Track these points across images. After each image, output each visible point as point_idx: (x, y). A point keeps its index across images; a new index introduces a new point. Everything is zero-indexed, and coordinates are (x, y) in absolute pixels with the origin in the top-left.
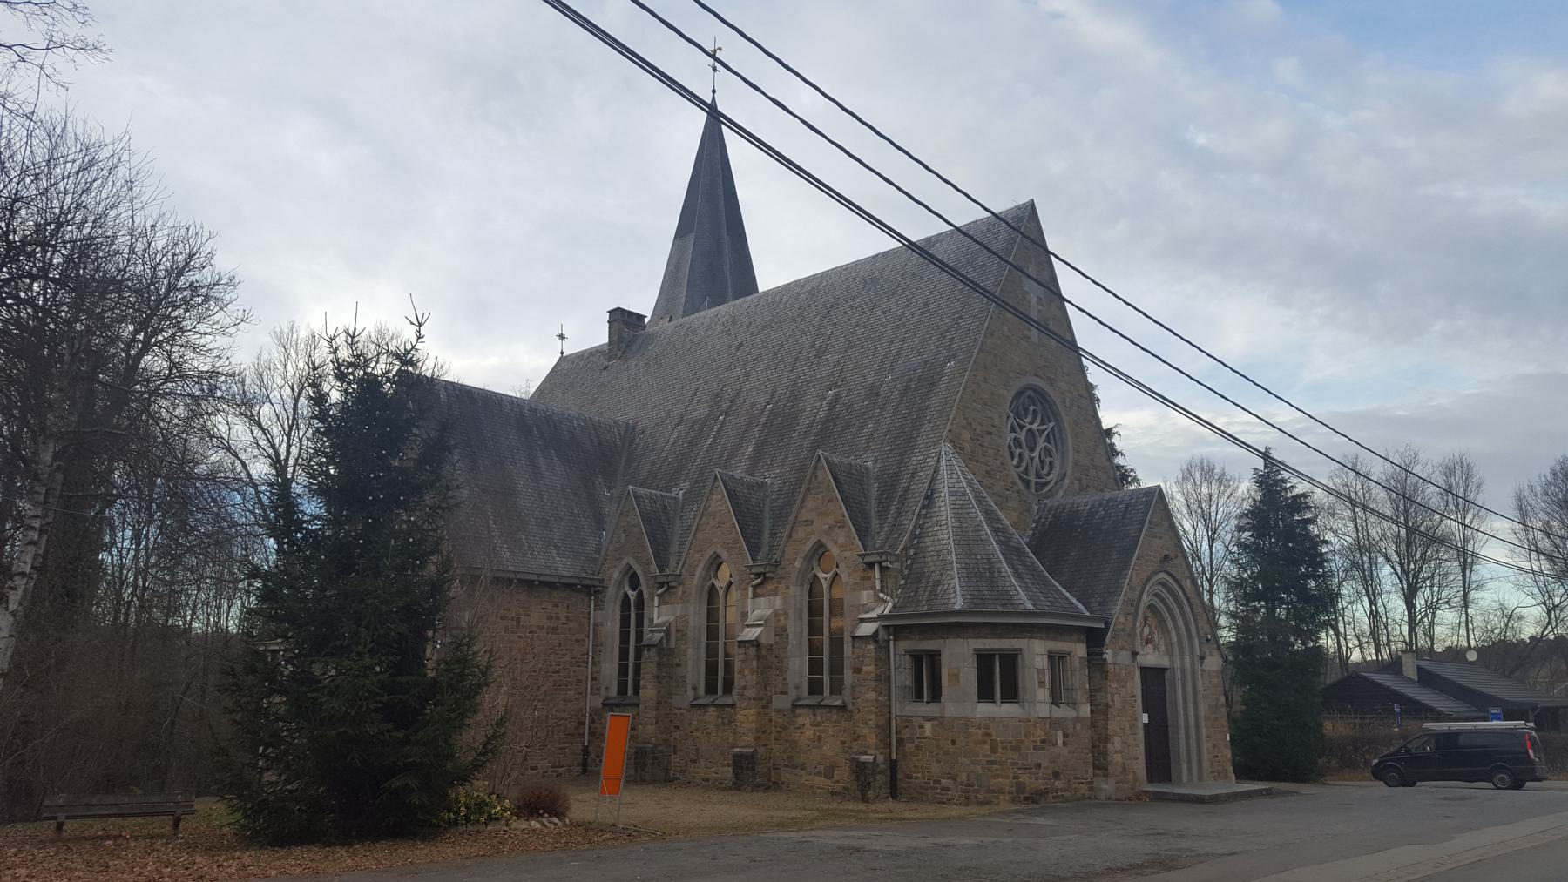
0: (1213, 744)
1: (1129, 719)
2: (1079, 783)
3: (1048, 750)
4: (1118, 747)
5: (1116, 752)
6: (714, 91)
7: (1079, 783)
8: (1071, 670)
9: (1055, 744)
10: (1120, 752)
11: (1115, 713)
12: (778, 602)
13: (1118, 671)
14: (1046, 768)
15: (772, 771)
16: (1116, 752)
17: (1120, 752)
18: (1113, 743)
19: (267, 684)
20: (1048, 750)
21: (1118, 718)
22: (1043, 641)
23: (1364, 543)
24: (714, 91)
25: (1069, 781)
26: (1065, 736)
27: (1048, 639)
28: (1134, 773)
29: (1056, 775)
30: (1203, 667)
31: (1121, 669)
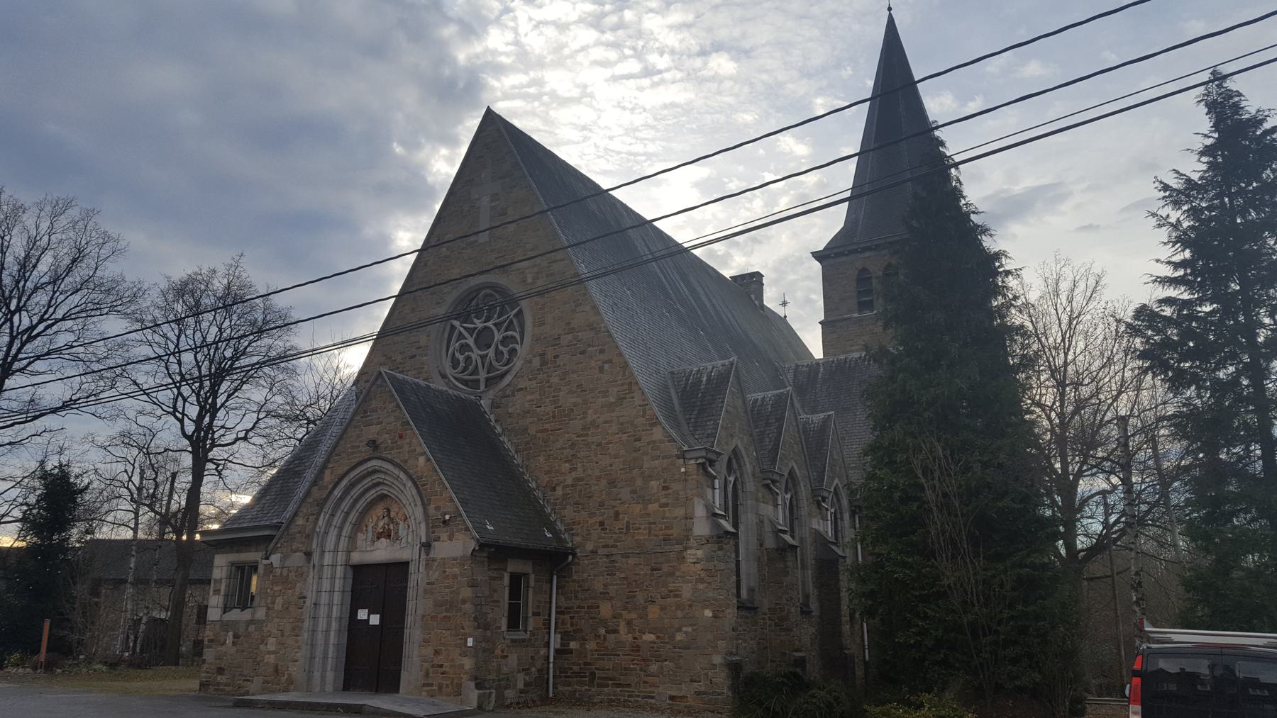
0: (436, 651)
1: (291, 620)
2: (245, 680)
3: (216, 648)
4: (271, 647)
5: (269, 653)
6: (890, 9)
7: (245, 680)
8: (230, 579)
9: (224, 643)
10: (273, 653)
11: (274, 615)
12: (210, 526)
13: (285, 574)
14: (211, 664)
15: (611, 667)
16: (269, 653)
17: (273, 653)
18: (266, 644)
19: (1201, 455)
20: (216, 648)
21: (276, 620)
22: (225, 555)
23: (1264, 260)
24: (890, 9)
25: (234, 676)
26: (236, 636)
27: (231, 552)
28: (289, 675)
29: (220, 671)
30: (431, 556)
31: (289, 571)
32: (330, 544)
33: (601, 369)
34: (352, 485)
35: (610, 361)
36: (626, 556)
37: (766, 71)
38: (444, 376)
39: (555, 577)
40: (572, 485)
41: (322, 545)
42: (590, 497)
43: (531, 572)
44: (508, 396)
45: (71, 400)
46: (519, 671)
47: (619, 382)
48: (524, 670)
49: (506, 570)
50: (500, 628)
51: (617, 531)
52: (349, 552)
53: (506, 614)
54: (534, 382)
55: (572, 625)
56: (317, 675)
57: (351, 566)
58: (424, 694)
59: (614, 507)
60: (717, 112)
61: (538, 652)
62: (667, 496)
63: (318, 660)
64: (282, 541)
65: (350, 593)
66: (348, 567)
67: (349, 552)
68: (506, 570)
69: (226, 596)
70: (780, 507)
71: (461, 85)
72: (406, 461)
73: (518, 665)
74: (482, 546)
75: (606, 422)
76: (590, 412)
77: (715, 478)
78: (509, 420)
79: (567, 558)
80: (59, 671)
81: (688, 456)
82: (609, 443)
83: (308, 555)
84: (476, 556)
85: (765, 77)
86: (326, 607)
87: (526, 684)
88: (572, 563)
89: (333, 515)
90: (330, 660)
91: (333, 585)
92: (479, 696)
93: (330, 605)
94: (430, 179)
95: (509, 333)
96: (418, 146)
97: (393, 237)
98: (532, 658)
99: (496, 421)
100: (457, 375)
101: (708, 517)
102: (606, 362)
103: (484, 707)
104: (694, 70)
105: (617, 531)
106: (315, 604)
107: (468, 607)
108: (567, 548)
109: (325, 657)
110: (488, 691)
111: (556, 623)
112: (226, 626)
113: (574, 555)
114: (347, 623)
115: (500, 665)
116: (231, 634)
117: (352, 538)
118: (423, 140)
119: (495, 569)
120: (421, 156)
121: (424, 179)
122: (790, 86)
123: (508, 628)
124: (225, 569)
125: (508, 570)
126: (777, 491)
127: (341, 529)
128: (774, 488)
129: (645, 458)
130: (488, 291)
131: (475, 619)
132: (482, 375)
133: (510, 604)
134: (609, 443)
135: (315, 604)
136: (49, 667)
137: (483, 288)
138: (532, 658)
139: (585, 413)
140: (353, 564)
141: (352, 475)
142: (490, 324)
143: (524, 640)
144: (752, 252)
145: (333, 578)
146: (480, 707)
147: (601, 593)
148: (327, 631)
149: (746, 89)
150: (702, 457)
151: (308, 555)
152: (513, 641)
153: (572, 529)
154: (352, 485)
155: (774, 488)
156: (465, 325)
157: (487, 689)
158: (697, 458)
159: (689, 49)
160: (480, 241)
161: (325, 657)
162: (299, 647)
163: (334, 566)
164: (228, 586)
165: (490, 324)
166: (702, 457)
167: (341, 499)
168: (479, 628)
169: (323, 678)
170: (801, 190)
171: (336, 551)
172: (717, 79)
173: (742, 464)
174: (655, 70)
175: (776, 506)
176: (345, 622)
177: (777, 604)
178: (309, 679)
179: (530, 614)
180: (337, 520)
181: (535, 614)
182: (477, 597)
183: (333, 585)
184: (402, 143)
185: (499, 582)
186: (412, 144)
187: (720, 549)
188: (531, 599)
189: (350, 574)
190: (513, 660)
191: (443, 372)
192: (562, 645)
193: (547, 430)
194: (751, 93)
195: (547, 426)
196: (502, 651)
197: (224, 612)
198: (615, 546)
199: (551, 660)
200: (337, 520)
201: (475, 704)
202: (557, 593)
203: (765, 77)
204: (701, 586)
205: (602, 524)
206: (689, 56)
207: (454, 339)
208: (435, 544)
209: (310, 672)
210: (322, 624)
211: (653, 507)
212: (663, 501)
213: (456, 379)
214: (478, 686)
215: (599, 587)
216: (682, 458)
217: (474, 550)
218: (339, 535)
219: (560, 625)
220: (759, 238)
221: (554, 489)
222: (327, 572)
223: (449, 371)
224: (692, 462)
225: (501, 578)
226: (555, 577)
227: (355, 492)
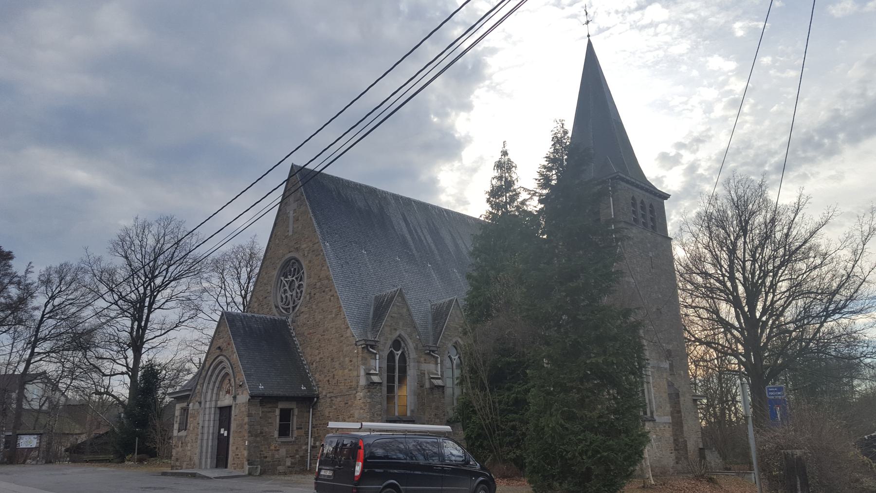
4: (189, 448)
30: (236, 402)
32: (208, 398)
33: (330, 300)
34: (215, 369)
35: (333, 296)
36: (336, 397)
37: (692, 11)
38: (277, 307)
39: (311, 409)
40: (319, 362)
41: (205, 398)
42: (325, 367)
43: (295, 407)
44: (298, 316)
45: (180, 322)
46: (287, 457)
47: (336, 307)
48: (290, 456)
49: (277, 407)
50: (273, 436)
51: (334, 385)
52: (216, 401)
53: (278, 429)
54: (306, 308)
55: (317, 434)
56: (204, 460)
57: (218, 408)
58: (233, 468)
59: (333, 372)
60: (657, 49)
61: (301, 448)
62: (351, 365)
63: (204, 454)
64: (193, 396)
65: (218, 421)
66: (217, 409)
67: (216, 401)
68: (277, 407)
69: (180, 424)
70: (439, 365)
71: (470, 67)
72: (230, 356)
73: (286, 454)
74: (253, 397)
75: (331, 328)
76: (326, 323)
77: (376, 354)
78: (298, 328)
79: (314, 399)
80: (146, 463)
81: (358, 344)
82: (332, 339)
83: (200, 403)
84: (251, 402)
85: (691, 16)
86: (207, 428)
87: (292, 463)
88: (316, 402)
89: (209, 383)
90: (209, 453)
91: (210, 417)
92: (249, 469)
93: (209, 427)
94: (457, 135)
95: (301, 282)
96: (447, 115)
97: (438, 178)
98: (297, 450)
99: (294, 329)
100: (283, 306)
101: (365, 375)
102: (331, 296)
103: (253, 473)
104: (634, 21)
105: (334, 385)
106: (203, 427)
107: (246, 427)
108: (314, 395)
109: (207, 452)
110: (256, 466)
111: (311, 433)
112: (179, 438)
113: (318, 398)
114: (217, 435)
115: (273, 454)
116: (180, 442)
117: (218, 394)
118: (449, 110)
119: (269, 407)
120: (449, 121)
121: (453, 136)
122: (713, 19)
123: (279, 436)
124: (179, 411)
125: (279, 407)
126: (437, 356)
127: (213, 390)
128: (435, 355)
129: (345, 345)
130: (293, 261)
131: (249, 432)
132: (291, 305)
133: (280, 424)
134: (332, 339)
135: (203, 427)
136: (140, 461)
137: (293, 259)
138: (297, 450)
139: (324, 323)
140: (219, 406)
141: (214, 363)
142: (294, 278)
143: (291, 442)
144: (697, 150)
145: (210, 414)
146: (250, 474)
147: (328, 417)
148: (208, 439)
149: (677, 28)
150: (364, 344)
151: (200, 403)
152: (282, 442)
153: (318, 384)
154: (215, 369)
155: (435, 355)
156: (286, 279)
157: (255, 465)
158: (362, 345)
159: (629, 7)
160: (289, 235)
161: (207, 452)
162: (197, 448)
163: (210, 408)
164: (180, 419)
165: (294, 278)
166: (364, 344)
167: (211, 376)
168: (252, 436)
169: (206, 462)
170: (733, 97)
171: (211, 401)
172: (653, 25)
173: (407, 344)
174: (605, 28)
175: (437, 364)
176: (216, 435)
177: (430, 418)
178: (200, 463)
179: (295, 429)
180: (211, 386)
181: (297, 429)
182: (251, 421)
183: (210, 417)
184: (437, 115)
185: (272, 414)
186: (443, 115)
187: (369, 392)
188: (295, 422)
189: (218, 411)
190: (283, 451)
191: (277, 305)
192: (314, 444)
193: (311, 333)
194: (682, 29)
195: (311, 331)
196: (275, 447)
197: (179, 432)
198: (333, 392)
199: (309, 451)
200: (211, 386)
201: (247, 473)
202: (312, 418)
203: (691, 16)
204: (362, 411)
205: (328, 381)
206: (630, 12)
207: (282, 287)
208: (238, 396)
209: (201, 459)
210: (205, 437)
211: (346, 371)
212: (350, 368)
213: (282, 308)
214: (249, 464)
215: (327, 414)
216: (22, 388)
217: (249, 399)
218: (212, 393)
219: (313, 434)
220: (701, 138)
221: (312, 364)
222: (207, 412)
223: (280, 304)
224: (360, 347)
225: (274, 411)
226: (311, 409)
227: (217, 372)
